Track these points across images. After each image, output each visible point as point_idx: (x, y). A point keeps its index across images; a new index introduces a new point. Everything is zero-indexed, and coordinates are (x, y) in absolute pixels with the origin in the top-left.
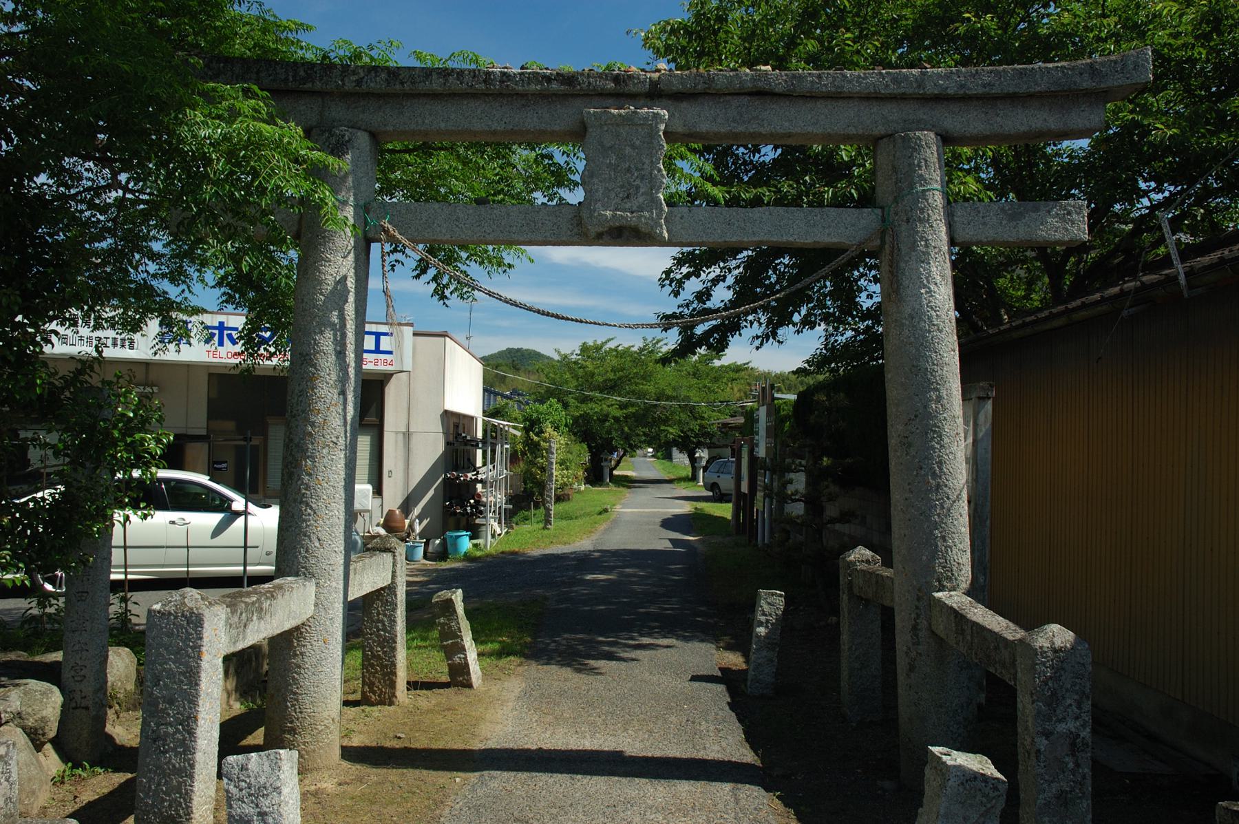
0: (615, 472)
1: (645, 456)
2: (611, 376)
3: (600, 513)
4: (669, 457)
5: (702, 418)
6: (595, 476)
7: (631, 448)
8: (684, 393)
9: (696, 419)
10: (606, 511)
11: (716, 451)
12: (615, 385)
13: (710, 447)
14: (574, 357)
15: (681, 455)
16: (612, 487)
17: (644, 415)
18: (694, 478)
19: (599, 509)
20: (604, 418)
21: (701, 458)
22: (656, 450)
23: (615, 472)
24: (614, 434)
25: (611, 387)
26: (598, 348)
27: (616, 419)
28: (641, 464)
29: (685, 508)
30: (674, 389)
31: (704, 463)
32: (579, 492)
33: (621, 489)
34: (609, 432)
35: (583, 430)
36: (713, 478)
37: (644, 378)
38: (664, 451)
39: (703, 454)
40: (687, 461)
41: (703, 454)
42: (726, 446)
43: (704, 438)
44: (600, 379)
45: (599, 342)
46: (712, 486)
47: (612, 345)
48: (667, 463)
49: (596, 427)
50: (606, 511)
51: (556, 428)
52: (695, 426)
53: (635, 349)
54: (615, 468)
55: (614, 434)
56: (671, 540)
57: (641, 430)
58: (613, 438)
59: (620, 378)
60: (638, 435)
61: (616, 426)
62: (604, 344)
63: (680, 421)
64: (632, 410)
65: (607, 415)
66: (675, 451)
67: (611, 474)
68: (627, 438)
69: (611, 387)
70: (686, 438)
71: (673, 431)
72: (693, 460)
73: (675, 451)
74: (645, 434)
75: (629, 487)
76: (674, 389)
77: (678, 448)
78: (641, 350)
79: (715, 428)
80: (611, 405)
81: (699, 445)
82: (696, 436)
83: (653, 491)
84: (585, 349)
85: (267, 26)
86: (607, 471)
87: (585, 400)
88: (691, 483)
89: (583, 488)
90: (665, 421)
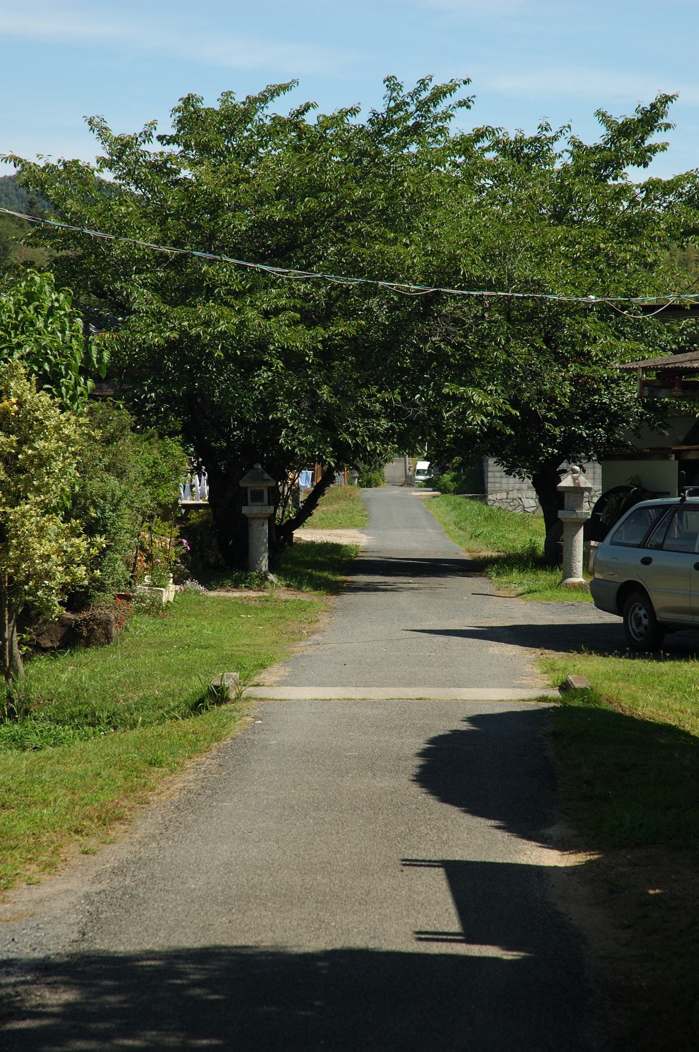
0: (302, 535)
1: (409, 482)
2: (277, 212)
3: (196, 707)
4: (475, 487)
5: (583, 358)
6: (217, 551)
7: (354, 459)
8: (522, 268)
9: (563, 361)
10: (218, 696)
11: (627, 470)
12: (293, 245)
13: (608, 454)
14: (153, 148)
15: (513, 482)
16: (278, 590)
17: (390, 346)
18: (552, 558)
19: (197, 685)
20: (248, 357)
21: (578, 491)
22: (439, 460)
23: (302, 535)
24: (285, 411)
25: (281, 244)
26: (235, 117)
27: (293, 359)
28: (390, 510)
29: (516, 683)
30: (491, 258)
31: (587, 509)
32: (155, 609)
33: (307, 596)
34: (267, 404)
35: (173, 393)
36: (626, 563)
37: (387, 219)
38: (461, 467)
39: (584, 479)
40: (530, 499)
41: (584, 479)
42: (662, 453)
43: (588, 425)
44: (242, 222)
45: (239, 98)
46: (624, 596)
47: (281, 107)
48: (472, 506)
49: (220, 387)
50: (218, 696)
51: (48, 380)
52: (560, 382)
53: (361, 120)
54: (299, 521)
55: (285, 411)
56: (464, 878)
57: (376, 398)
58: (280, 424)
59: (309, 219)
60: (366, 413)
61: (292, 383)
62: (254, 103)
63: (508, 369)
64: (343, 327)
65: (262, 345)
66: (494, 471)
67: (281, 535)
68: (328, 423)
69: (281, 244)
70: (529, 423)
71: (485, 400)
72: (552, 500)
73: (494, 471)
74: (393, 412)
75: (336, 589)
76: (491, 258)
77: (502, 458)
78: (381, 124)
79: (630, 392)
80: (266, 313)
81: (572, 449)
82: (564, 418)
83: (417, 603)
84: (190, 117)
85: (688, 661)
86: (261, 535)
87: (186, 289)
88: (545, 578)
89: (169, 592)
90: (464, 370)
